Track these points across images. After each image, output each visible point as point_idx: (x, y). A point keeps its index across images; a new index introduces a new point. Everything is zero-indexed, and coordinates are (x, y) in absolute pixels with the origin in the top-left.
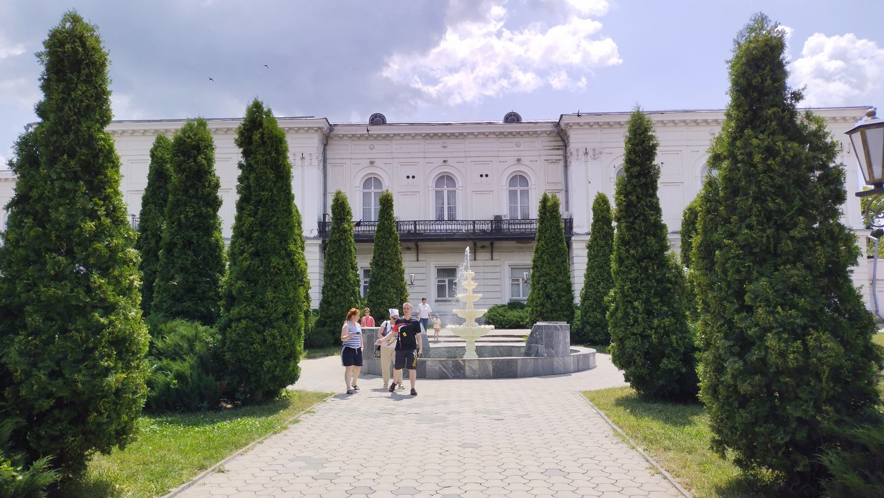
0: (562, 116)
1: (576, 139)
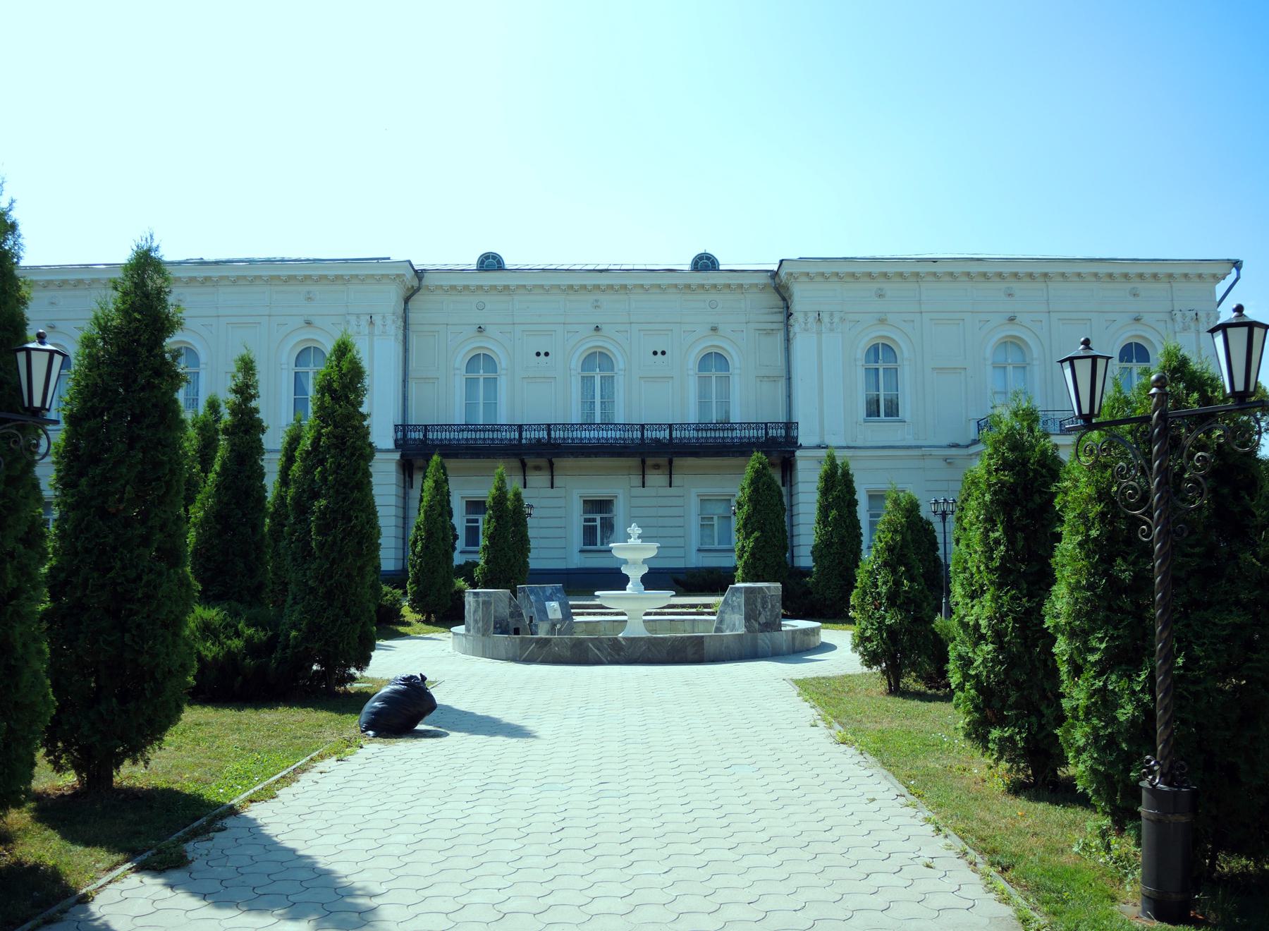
0: (781, 261)
1: (802, 298)
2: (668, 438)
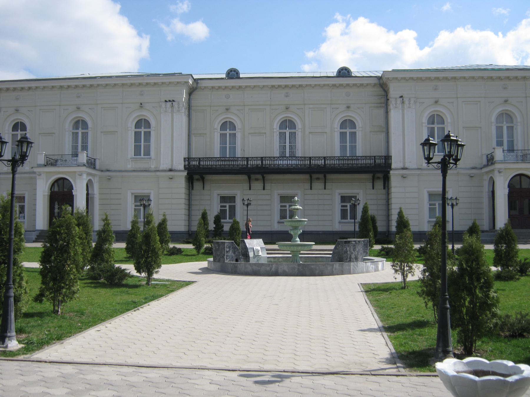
1: (394, 92)
2: (323, 164)
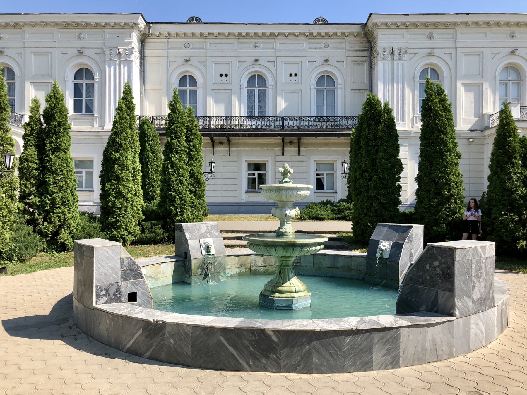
2: (298, 125)
